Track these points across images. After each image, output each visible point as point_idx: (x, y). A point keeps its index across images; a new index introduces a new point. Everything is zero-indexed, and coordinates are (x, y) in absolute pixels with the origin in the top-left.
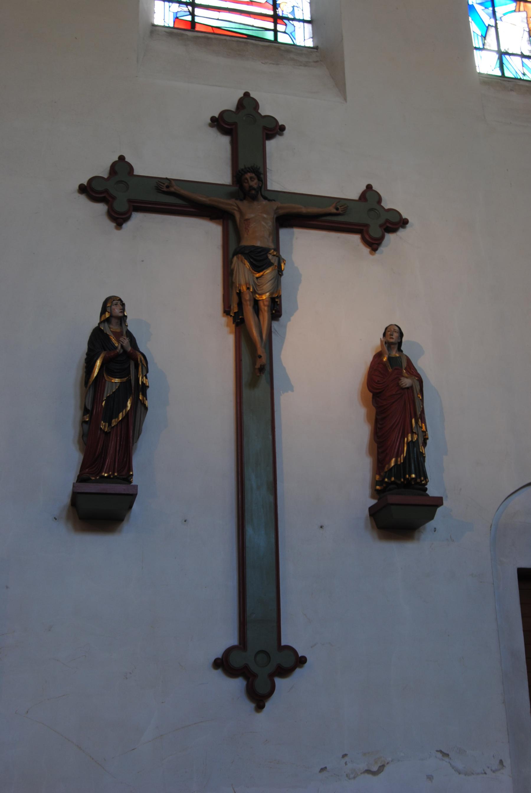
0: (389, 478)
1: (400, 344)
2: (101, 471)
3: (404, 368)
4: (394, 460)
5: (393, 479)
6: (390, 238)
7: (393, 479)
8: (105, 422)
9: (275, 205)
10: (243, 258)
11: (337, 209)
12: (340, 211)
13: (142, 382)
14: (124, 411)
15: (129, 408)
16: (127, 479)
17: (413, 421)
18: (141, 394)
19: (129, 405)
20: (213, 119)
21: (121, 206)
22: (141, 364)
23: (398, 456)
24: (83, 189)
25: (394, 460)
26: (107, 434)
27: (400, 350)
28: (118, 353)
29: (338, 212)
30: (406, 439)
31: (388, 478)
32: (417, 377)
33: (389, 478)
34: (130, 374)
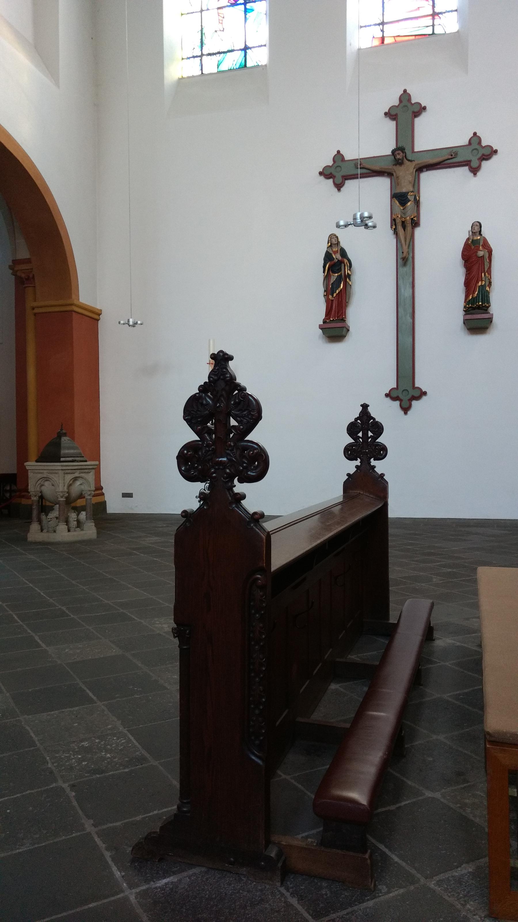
0: (469, 305)
1: (480, 231)
2: (330, 318)
3: (481, 245)
4: (471, 296)
5: (470, 305)
6: (485, 164)
7: (470, 305)
8: (331, 295)
9: (414, 164)
10: (396, 200)
11: (452, 155)
12: (453, 156)
13: (348, 273)
14: (339, 289)
15: (342, 287)
16: (343, 320)
17: (483, 274)
18: (347, 279)
19: (342, 285)
20: (386, 114)
21: (339, 180)
22: (346, 265)
23: (474, 293)
24: (321, 173)
25: (471, 296)
26: (332, 300)
27: (480, 234)
28: (335, 262)
29: (452, 157)
30: (478, 284)
31: (468, 305)
32: (487, 249)
33: (469, 305)
34: (341, 270)
